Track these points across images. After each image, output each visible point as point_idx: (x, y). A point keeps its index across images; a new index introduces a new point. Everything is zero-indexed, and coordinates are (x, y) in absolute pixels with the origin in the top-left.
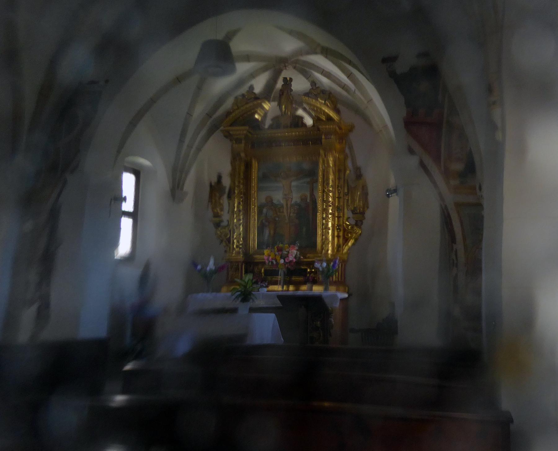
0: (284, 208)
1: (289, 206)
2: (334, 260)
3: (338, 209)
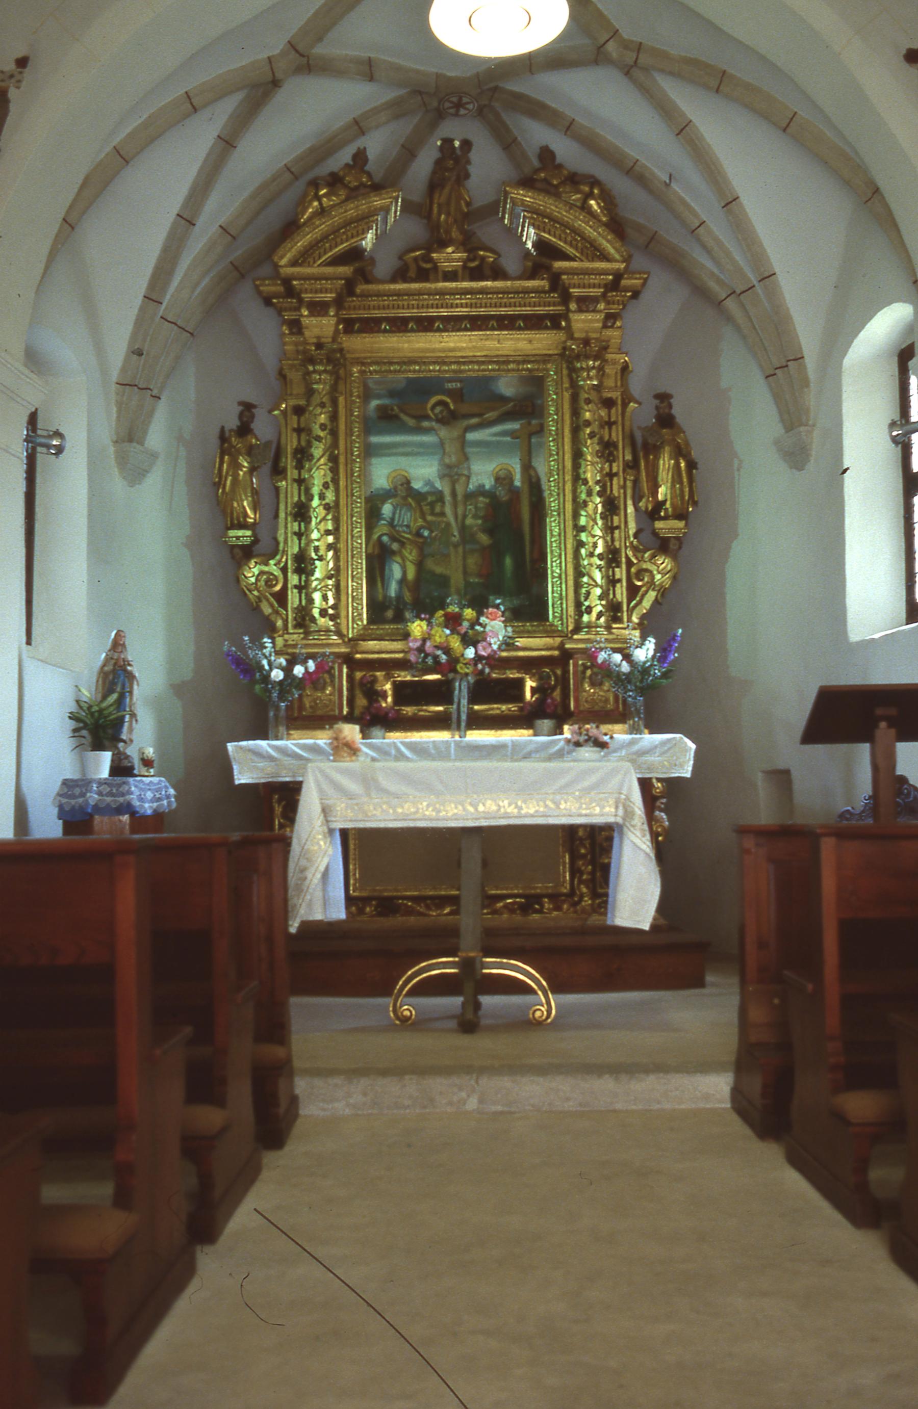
0: (447, 504)
1: (460, 498)
2: (434, 534)
3: (611, 507)
